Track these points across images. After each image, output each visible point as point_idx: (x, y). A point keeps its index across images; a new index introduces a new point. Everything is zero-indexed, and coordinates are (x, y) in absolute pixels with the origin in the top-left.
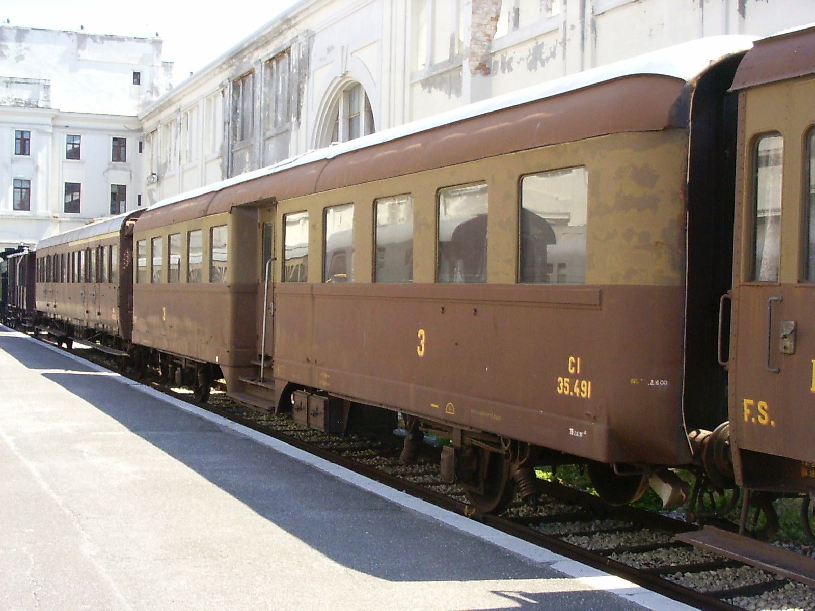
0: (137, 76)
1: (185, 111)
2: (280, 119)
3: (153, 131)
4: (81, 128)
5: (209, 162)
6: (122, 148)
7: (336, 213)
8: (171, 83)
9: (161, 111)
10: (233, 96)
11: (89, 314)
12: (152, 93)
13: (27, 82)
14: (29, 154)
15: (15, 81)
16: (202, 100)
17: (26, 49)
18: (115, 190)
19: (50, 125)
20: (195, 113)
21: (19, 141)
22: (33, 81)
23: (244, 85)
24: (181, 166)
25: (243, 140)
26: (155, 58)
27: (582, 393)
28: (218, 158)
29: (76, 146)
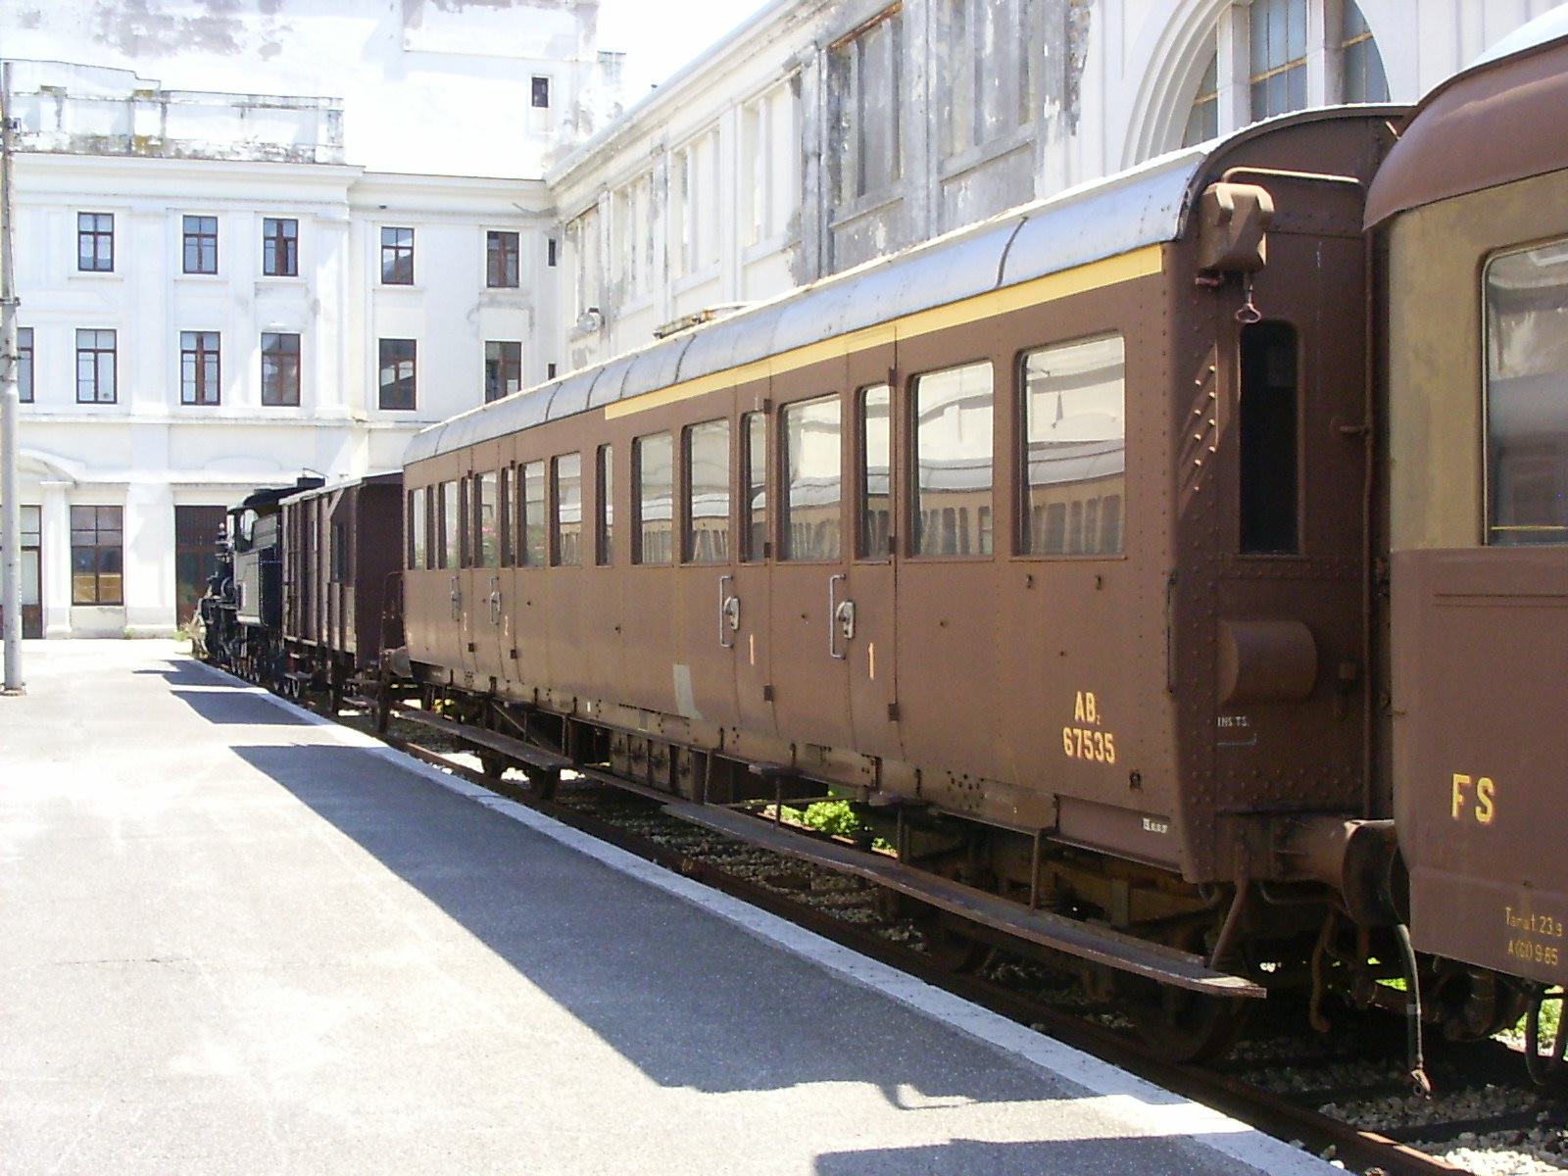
0: (540, 90)
1: (676, 150)
2: (990, 120)
3: (584, 213)
4: (416, 211)
5: (683, 293)
6: (510, 256)
7: (1036, 395)
8: (620, 102)
9: (607, 159)
10: (829, 87)
11: (519, 660)
12: (576, 126)
13: (287, 105)
14: (296, 274)
15: (261, 102)
16: (732, 112)
17: (284, 28)
18: (496, 355)
19: (343, 204)
20: (706, 150)
21: (273, 243)
22: (302, 103)
23: (861, 54)
24: (669, 282)
25: (863, 194)
26: (581, 43)
27: (1086, 751)
28: (784, 251)
29: (403, 253)
